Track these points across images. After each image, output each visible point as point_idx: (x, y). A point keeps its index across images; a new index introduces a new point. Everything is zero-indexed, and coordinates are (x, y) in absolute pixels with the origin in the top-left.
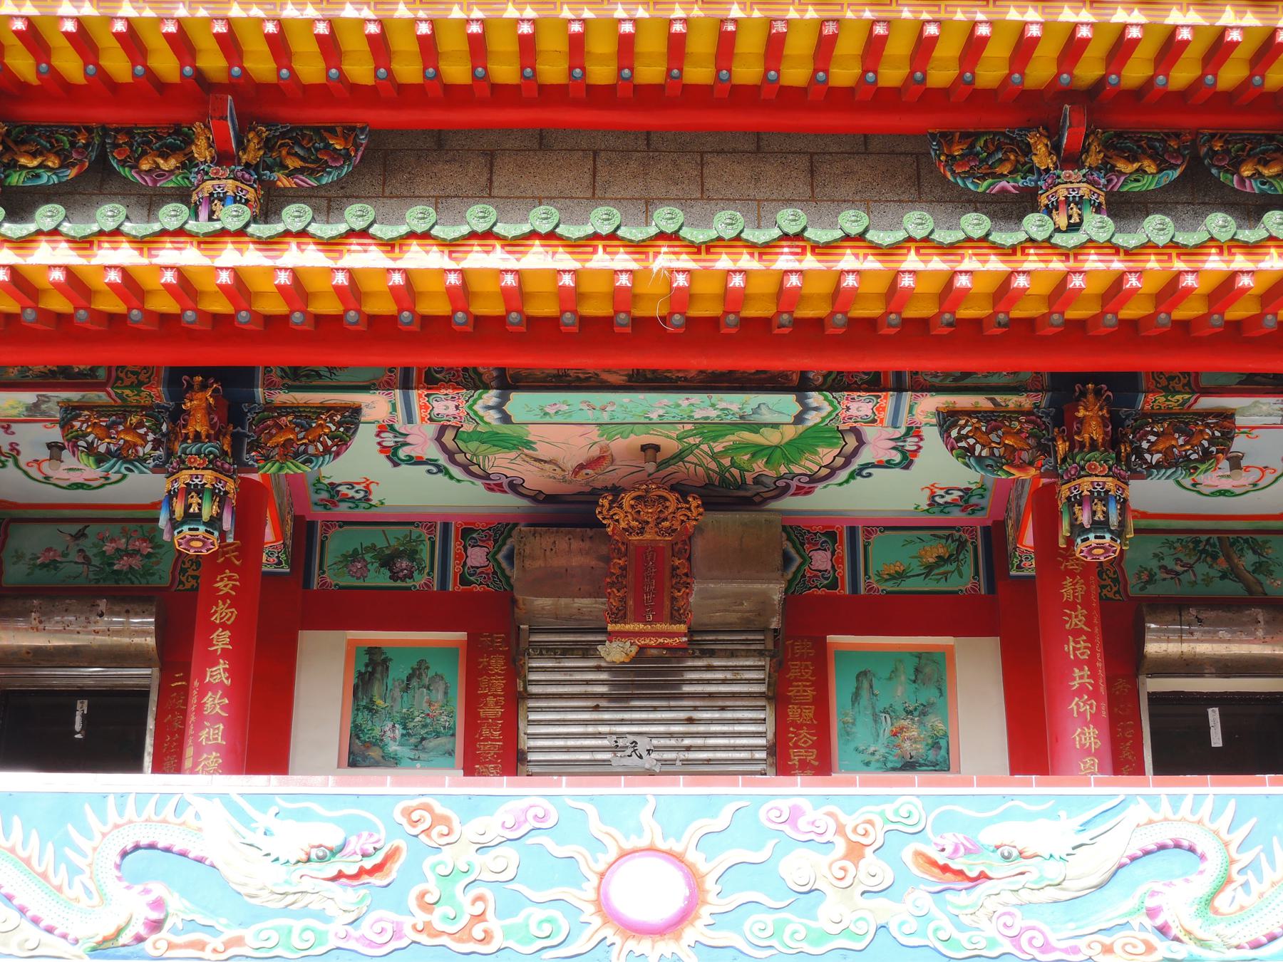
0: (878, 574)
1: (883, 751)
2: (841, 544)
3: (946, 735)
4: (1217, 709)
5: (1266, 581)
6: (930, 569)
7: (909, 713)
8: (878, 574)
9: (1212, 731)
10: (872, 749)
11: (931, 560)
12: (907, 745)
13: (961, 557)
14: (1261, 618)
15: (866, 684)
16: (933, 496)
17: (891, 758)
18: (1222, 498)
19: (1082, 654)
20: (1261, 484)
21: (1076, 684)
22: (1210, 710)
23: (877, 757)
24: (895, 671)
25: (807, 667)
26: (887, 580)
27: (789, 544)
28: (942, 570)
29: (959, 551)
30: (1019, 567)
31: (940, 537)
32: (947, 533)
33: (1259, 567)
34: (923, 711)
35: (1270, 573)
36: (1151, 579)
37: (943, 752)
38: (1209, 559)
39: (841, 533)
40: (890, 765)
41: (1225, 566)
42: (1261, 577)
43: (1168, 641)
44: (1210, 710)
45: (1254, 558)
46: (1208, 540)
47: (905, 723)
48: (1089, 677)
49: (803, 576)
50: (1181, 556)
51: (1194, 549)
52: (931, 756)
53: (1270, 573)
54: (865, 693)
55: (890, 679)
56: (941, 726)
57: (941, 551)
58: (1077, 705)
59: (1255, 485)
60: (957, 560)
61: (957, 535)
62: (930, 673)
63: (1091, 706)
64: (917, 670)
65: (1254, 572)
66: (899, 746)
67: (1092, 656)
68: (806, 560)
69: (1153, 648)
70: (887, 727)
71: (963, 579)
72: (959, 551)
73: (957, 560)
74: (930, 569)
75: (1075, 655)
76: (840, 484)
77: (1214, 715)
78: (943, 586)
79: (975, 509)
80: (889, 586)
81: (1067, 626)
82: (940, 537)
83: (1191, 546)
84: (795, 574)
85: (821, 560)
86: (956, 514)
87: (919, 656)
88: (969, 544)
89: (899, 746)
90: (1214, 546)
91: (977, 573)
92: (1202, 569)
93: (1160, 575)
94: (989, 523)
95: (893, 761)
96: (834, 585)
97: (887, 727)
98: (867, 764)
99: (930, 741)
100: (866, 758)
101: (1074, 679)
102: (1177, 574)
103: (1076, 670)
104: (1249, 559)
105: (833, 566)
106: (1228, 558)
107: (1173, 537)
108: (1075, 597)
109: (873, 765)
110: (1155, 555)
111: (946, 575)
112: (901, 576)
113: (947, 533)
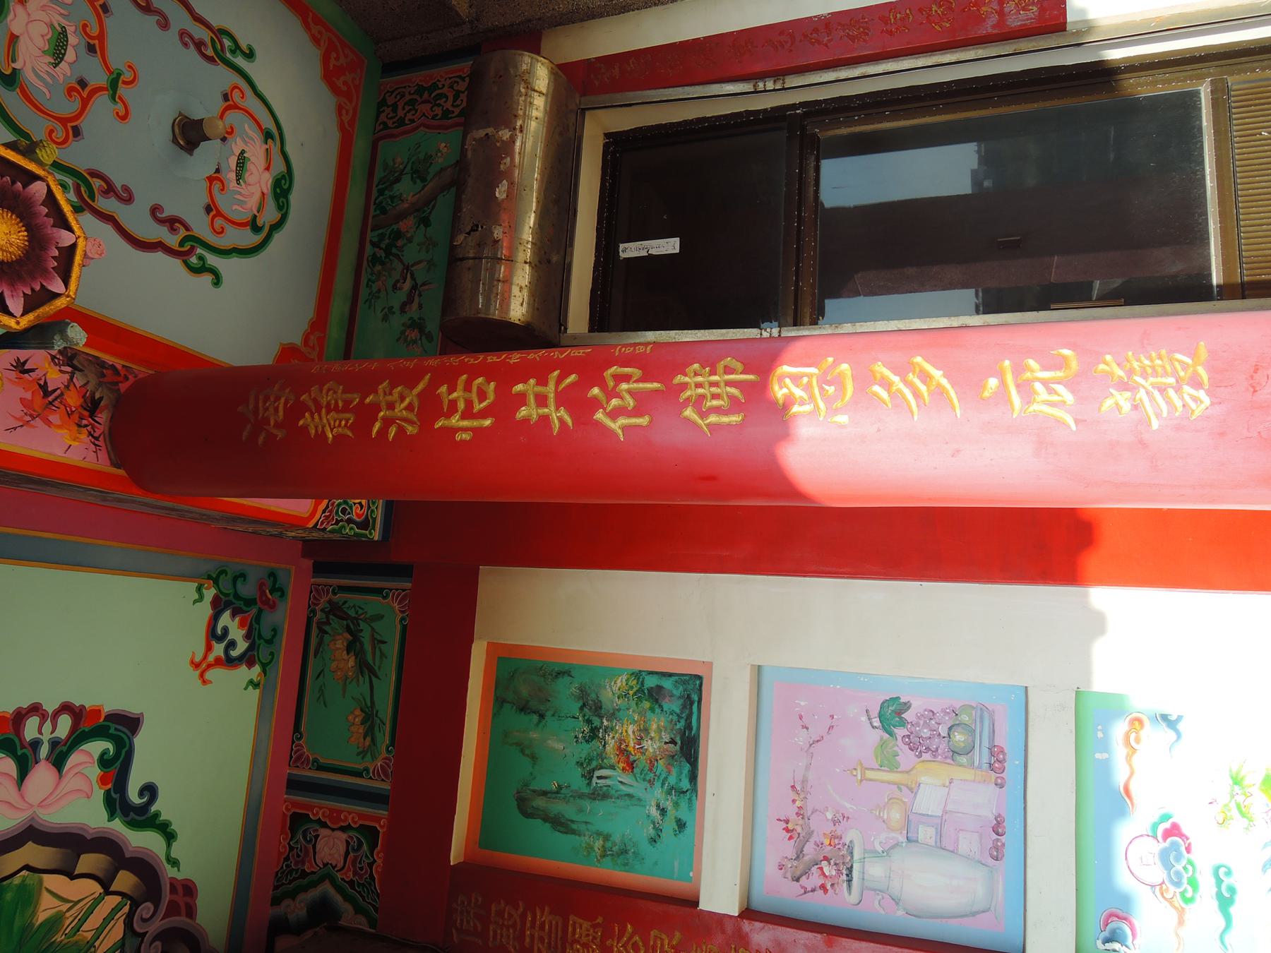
0: (363, 753)
1: (658, 793)
2: (311, 807)
3: (637, 675)
4: (622, 246)
5: (440, 162)
6: (365, 668)
7: (593, 734)
8: (363, 753)
9: (654, 252)
10: (654, 812)
11: (351, 663)
12: (651, 746)
13: (352, 613)
14: (482, 133)
15: (540, 802)
16: (229, 662)
17: (672, 780)
18: (293, 197)
19: (482, 395)
20: (268, 124)
21: (558, 416)
22: (623, 255)
23: (668, 805)
24: (522, 747)
25: (500, 913)
26: (373, 740)
27: (302, 896)
28: (368, 647)
29: (343, 616)
30: (365, 525)
31: (320, 643)
32: (315, 631)
33: (419, 174)
34: (592, 707)
35: (428, 159)
36: (418, 325)
37: (667, 684)
38: (400, 243)
39: (295, 804)
40: (685, 784)
41: (411, 221)
42: (433, 170)
43: (508, 281)
44: (623, 255)
45: (406, 179)
46: (374, 244)
47: (611, 744)
48: (543, 382)
49: (351, 883)
50: (391, 282)
51: (383, 264)
52: (675, 706)
53: (428, 159)
54: (557, 807)
55: (533, 758)
56: (621, 681)
57: (340, 644)
58: (614, 415)
59: (268, 136)
60: (356, 620)
61: (319, 616)
62: (531, 685)
63: (619, 379)
64: (524, 708)
65: (423, 180)
66: (652, 762)
67: (489, 373)
68: (327, 875)
69: (518, 310)
70: (616, 778)
71: (386, 613)
72: (343, 616)
73: (356, 620)
74: (365, 668)
75: (483, 414)
76: (170, 837)
77: (631, 250)
78: (392, 649)
79: (273, 588)
80: (384, 738)
81: (411, 430)
82: (320, 643)
83: (378, 267)
84: (347, 898)
85: (331, 847)
86: (284, 617)
87: (500, 701)
88: (336, 598)
89: (652, 762)
90: (382, 237)
91: (378, 591)
92: (411, 253)
93: (413, 312)
94: (308, 563)
95: (679, 776)
96: (370, 833)
97: (616, 778)
98: (681, 825)
99: (647, 704)
100: (669, 826)
101: (545, 419)
102: (414, 287)
103: (523, 412)
104: (407, 190)
105: (343, 829)
106: (402, 216)
107: (364, 293)
108: (346, 409)
109: (683, 814)
110: (385, 319)
111: (378, 642)
112: (369, 717)
113: (315, 631)
